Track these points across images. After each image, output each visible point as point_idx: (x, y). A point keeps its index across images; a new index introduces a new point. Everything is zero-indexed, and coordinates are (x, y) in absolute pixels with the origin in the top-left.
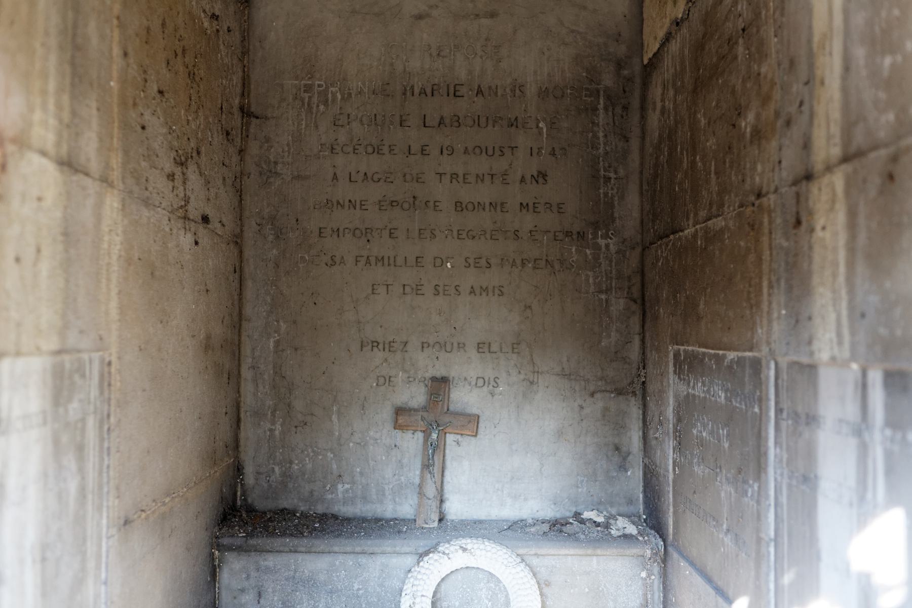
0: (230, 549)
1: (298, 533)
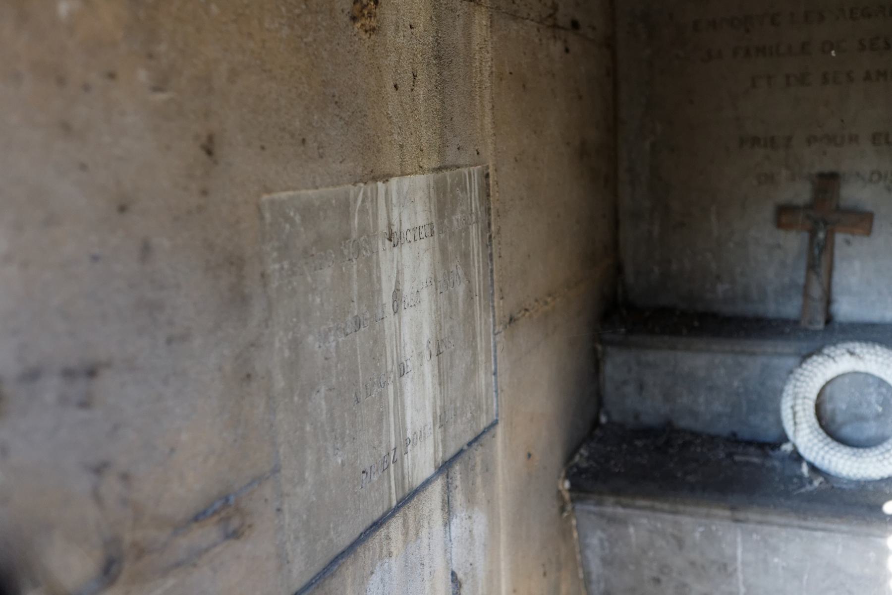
0: (612, 343)
1: (675, 332)
